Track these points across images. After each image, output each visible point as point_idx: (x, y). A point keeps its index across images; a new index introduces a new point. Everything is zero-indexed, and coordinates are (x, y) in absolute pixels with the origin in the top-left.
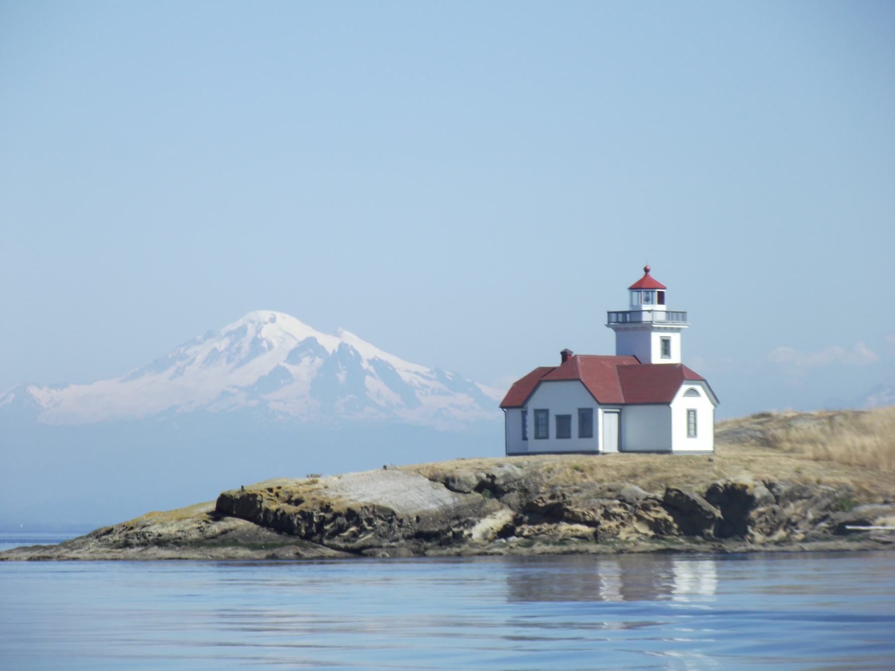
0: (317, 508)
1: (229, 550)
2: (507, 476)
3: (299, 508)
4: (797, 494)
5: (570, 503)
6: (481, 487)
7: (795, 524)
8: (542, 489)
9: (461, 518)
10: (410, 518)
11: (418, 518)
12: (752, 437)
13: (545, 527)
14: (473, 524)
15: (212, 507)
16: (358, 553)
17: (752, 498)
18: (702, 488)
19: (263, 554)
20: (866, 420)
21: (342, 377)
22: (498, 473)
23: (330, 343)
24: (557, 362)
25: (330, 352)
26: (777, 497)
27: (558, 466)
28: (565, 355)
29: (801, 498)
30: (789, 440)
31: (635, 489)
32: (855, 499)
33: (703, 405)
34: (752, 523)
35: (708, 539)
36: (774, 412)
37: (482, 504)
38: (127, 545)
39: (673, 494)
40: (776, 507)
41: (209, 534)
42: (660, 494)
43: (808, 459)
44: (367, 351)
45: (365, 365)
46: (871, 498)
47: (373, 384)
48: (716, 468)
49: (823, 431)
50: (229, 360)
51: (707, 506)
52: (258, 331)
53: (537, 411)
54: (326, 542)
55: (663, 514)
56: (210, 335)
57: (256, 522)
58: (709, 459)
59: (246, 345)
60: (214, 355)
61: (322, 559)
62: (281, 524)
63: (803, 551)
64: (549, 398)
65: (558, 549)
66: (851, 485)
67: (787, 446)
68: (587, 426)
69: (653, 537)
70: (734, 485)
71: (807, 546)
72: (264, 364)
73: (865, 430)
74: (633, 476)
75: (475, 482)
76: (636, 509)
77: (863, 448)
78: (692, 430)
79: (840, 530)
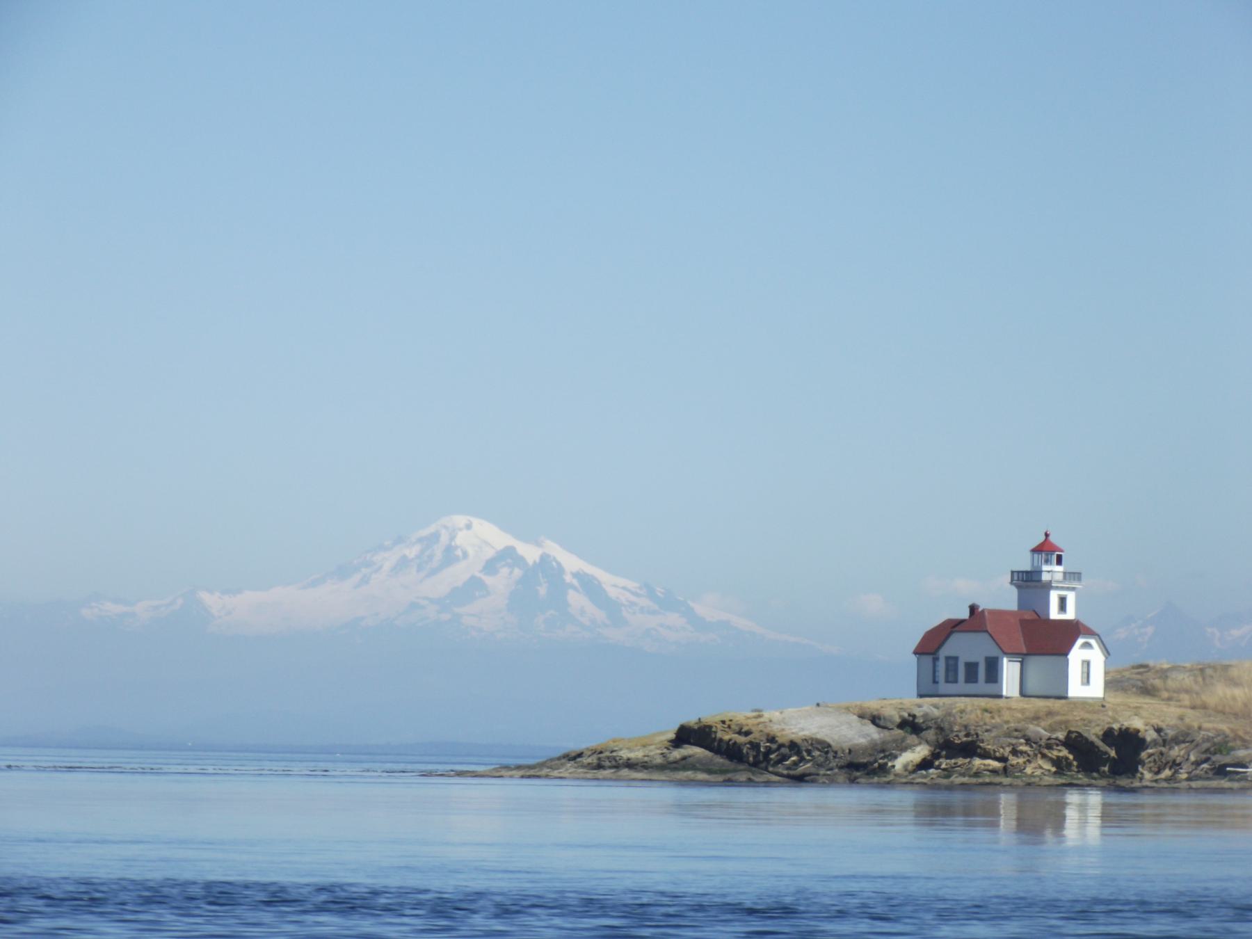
0: (764, 739)
1: (690, 774)
2: (925, 715)
3: (750, 738)
4: (1183, 738)
5: (983, 741)
7: (1179, 764)
8: (956, 728)
9: (887, 751)
10: (843, 751)
11: (850, 751)
12: (1133, 686)
13: (960, 761)
14: (896, 757)
15: (672, 736)
16: (800, 779)
17: (1143, 740)
18: (1099, 731)
19: (720, 778)
20: (1234, 672)
21: (543, 591)
22: (918, 712)
23: (531, 554)
24: (964, 614)
25: (530, 562)
26: (1164, 741)
27: (969, 708)
28: (973, 609)
29: (1184, 742)
30: (1167, 690)
31: (1039, 730)
32: (1230, 744)
33: (1096, 656)
34: (1142, 763)
36: (1151, 663)
37: (903, 739)
38: (599, 767)
39: (1073, 735)
40: (1163, 749)
42: (1061, 735)
43: (1185, 707)
44: (571, 563)
45: (568, 578)
47: (576, 599)
48: (1110, 713)
49: (1196, 682)
50: (419, 570)
51: (1104, 747)
52: (452, 538)
53: (948, 658)
54: (771, 769)
55: (1064, 752)
56: (399, 540)
57: (706, 748)
58: (1101, 705)
59: (438, 551)
60: (404, 562)
61: (768, 784)
62: (732, 752)
63: (1191, 788)
64: (966, 648)
65: (974, 780)
66: (1228, 732)
67: (1165, 695)
69: (1055, 773)
70: (1127, 729)
71: (1194, 784)
72: (458, 574)
73: (1234, 682)
74: (1036, 718)
75: (898, 720)
76: (1041, 747)
77: (1234, 698)
78: (1087, 680)
79: (1220, 771)
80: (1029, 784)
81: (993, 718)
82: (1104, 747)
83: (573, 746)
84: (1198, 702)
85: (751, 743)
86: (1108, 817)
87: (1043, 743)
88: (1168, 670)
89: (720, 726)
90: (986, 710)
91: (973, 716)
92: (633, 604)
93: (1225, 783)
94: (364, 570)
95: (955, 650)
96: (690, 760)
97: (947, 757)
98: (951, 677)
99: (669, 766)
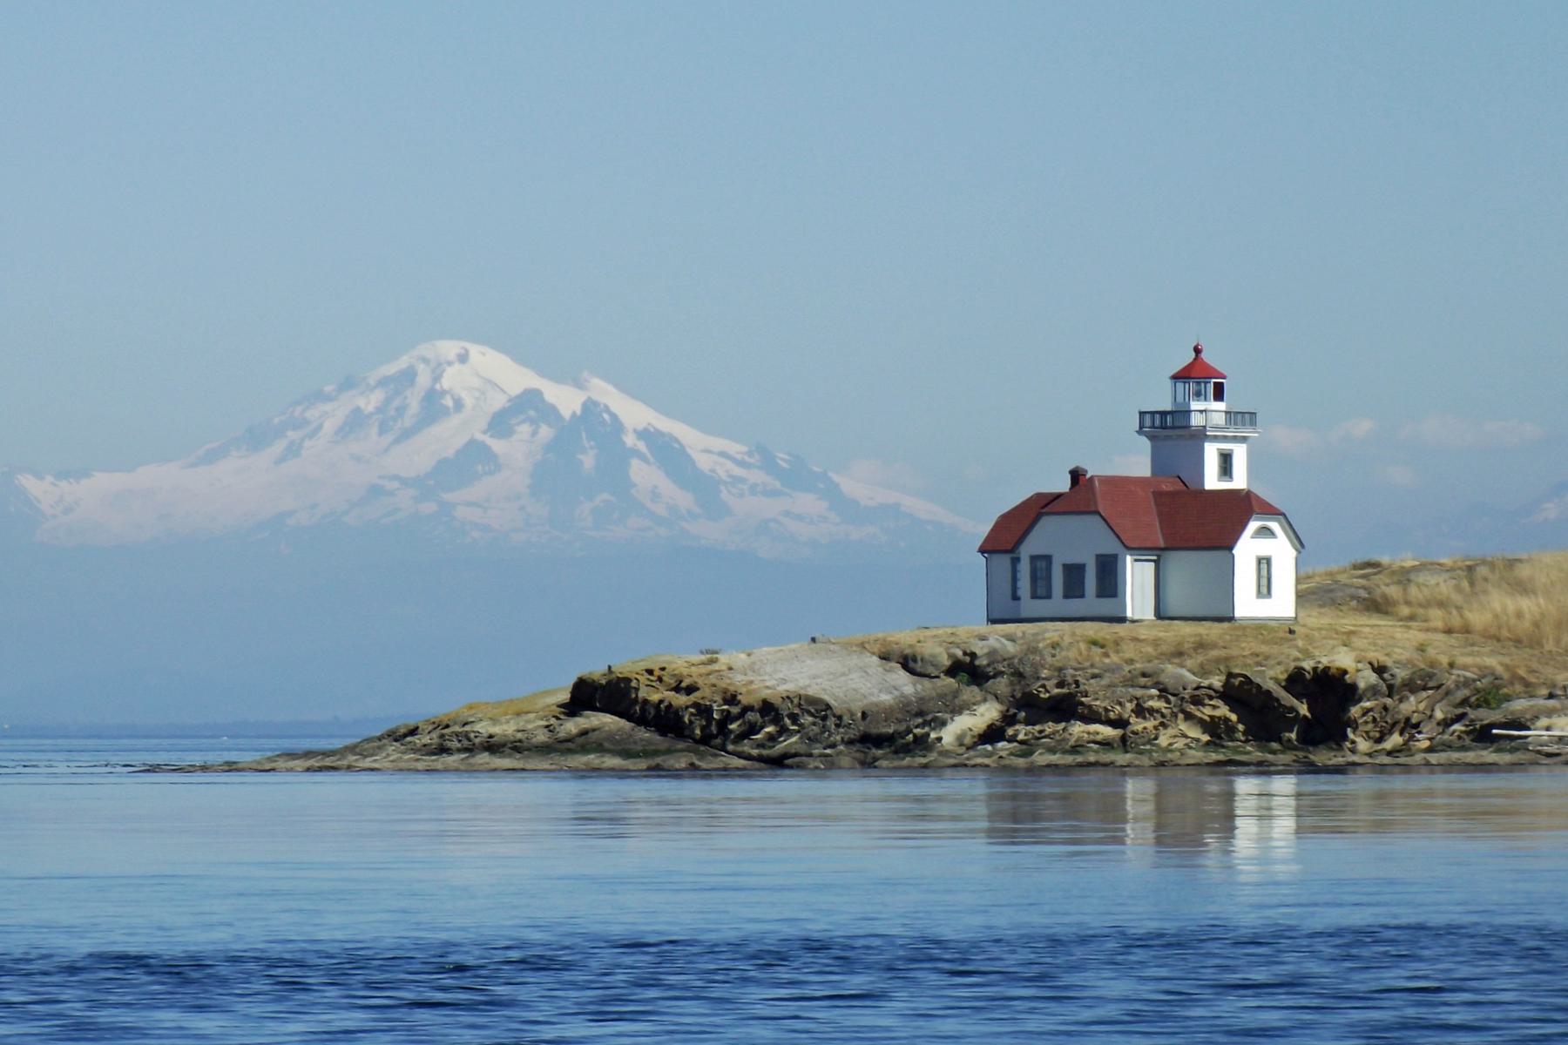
0: (718, 698)
2: (992, 653)
6: (955, 669)
7: (1417, 726)
8: (1045, 673)
9: (928, 714)
10: (852, 714)
12: (1353, 597)
13: (1049, 727)
14: (943, 724)
15: (565, 696)
16: (778, 763)
19: (643, 764)
20: (1524, 572)
21: (588, 461)
22: (980, 648)
23: (566, 400)
24: (1063, 485)
25: (566, 413)
26: (1390, 687)
27: (1067, 640)
28: (1076, 476)
29: (1425, 688)
30: (1408, 603)
31: (1183, 674)
33: (1281, 551)
34: (1354, 725)
35: (1288, 746)
36: (1385, 560)
37: (956, 694)
38: (442, 750)
39: (1236, 682)
41: (562, 735)
42: (1217, 681)
43: (1435, 630)
44: (634, 414)
45: (630, 440)
46: (1529, 689)
47: (644, 475)
49: (1458, 589)
50: (383, 430)
51: (1287, 699)
52: (437, 378)
53: (1034, 559)
54: (730, 747)
55: (1223, 711)
56: (348, 384)
57: (621, 716)
60: (355, 422)
61: (726, 773)
62: (665, 722)
63: (1428, 764)
65: (1069, 759)
66: (1500, 670)
67: (1405, 611)
68: (1109, 579)
69: (1208, 743)
70: (1327, 669)
71: (1433, 758)
72: (446, 437)
74: (1179, 654)
75: (947, 662)
76: (1185, 702)
77: (1519, 615)
78: (1265, 588)
79: (1483, 736)
80: (1162, 764)
81: (1106, 655)
82: (1287, 699)
83: (401, 717)
84: (1456, 621)
85: (696, 705)
86: (1316, 818)
87: (1186, 694)
88: (1414, 569)
89: (643, 679)
90: (1095, 643)
91: (1072, 654)
92: (737, 480)
93: (1488, 756)
94: (290, 433)
95: (1042, 545)
96: (593, 736)
97: (1028, 722)
98: (1041, 588)
99: (558, 747)
